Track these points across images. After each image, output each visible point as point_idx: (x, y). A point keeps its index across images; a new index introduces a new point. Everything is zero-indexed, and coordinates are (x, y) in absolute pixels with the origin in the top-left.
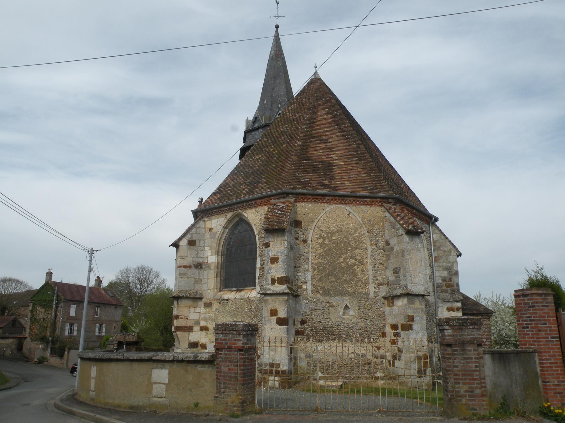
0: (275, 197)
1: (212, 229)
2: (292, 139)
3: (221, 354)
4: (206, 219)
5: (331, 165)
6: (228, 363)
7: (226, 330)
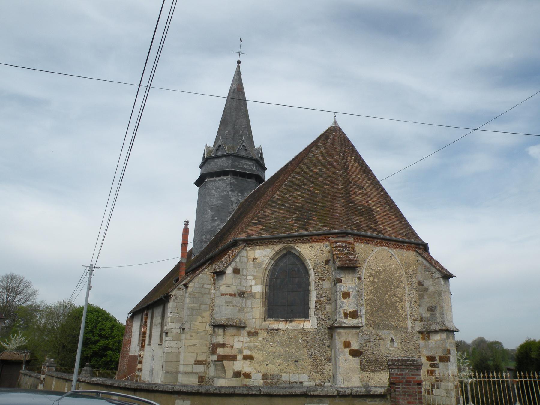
0: (334, 236)
1: (257, 259)
2: (332, 181)
3: (399, 388)
4: (248, 249)
5: (371, 210)
6: (406, 397)
7: (402, 365)
